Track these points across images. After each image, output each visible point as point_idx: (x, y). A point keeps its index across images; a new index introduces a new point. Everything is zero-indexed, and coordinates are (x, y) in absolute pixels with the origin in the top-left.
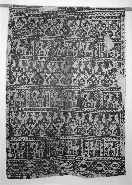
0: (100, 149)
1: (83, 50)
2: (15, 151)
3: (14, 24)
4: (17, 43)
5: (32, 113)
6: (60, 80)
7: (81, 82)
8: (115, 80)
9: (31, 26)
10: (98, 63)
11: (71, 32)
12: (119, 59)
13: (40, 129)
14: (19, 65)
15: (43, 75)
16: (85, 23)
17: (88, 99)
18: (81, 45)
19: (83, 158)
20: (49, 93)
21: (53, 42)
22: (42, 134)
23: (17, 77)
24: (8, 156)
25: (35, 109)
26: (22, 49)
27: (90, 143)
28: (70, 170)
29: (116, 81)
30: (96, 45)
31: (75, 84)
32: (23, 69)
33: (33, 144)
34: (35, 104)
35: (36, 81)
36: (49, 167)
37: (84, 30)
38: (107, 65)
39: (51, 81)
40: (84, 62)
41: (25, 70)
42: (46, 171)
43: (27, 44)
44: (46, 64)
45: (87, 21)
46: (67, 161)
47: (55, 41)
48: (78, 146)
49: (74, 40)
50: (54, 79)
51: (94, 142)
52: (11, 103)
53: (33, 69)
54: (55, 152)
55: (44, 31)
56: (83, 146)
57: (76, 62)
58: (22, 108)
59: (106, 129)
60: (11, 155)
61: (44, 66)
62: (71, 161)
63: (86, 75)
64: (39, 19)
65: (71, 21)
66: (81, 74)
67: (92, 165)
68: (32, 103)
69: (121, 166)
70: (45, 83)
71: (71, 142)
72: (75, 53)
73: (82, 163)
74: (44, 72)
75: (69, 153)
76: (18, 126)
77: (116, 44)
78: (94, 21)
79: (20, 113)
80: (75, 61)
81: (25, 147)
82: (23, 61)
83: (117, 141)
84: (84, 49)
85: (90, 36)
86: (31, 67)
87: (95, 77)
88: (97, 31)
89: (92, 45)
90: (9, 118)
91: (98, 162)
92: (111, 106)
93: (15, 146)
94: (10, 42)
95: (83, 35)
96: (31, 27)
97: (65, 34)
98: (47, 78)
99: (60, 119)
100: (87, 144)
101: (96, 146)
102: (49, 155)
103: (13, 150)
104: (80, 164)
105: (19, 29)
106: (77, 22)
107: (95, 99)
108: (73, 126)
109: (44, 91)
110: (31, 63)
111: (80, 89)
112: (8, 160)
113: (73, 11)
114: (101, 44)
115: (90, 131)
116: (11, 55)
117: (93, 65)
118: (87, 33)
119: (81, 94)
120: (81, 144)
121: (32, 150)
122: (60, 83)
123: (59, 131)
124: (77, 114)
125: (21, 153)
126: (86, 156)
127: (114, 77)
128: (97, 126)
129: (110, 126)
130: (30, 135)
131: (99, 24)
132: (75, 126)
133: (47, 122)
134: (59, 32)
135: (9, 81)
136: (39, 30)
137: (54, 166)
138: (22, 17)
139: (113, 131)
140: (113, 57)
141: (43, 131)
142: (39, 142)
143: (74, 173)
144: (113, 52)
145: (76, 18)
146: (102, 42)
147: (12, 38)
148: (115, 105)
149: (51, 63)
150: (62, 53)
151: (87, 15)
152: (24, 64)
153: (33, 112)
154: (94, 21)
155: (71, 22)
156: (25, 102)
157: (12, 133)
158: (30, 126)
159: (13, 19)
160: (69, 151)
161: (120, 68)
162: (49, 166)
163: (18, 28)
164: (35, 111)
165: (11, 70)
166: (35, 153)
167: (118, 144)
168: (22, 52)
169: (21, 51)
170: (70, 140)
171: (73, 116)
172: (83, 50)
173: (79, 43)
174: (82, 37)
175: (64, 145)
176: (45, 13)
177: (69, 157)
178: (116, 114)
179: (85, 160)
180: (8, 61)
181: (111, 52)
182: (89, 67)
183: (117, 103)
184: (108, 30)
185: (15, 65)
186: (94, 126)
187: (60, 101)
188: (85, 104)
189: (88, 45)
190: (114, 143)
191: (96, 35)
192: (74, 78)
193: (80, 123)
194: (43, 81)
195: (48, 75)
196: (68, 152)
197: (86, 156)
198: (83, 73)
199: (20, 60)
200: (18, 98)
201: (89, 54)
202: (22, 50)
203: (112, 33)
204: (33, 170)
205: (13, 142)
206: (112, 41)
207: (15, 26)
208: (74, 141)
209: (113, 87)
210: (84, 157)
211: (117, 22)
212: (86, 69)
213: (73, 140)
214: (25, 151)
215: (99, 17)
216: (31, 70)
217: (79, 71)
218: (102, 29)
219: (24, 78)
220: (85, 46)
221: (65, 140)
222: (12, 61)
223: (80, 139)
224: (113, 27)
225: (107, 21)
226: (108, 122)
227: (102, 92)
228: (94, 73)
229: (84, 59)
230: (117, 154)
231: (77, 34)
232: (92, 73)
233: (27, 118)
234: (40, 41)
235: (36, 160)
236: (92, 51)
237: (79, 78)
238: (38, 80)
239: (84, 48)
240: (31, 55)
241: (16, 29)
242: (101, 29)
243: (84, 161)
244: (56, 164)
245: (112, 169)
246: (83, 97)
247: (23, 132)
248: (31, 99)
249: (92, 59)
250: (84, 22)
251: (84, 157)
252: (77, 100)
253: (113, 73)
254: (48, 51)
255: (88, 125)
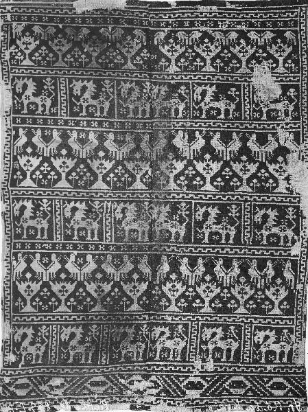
0: (240, 345)
1: (197, 103)
2: (24, 348)
3: (13, 42)
4: (25, 87)
5: (68, 255)
6: (138, 177)
7: (195, 182)
8: (286, 175)
9: (56, 45)
10: (238, 133)
11: (163, 60)
12: (295, 124)
13: (89, 294)
14: (35, 140)
15: (95, 164)
16: (202, 38)
17: (214, 223)
18: (194, 91)
19: (194, 368)
20: (111, 208)
21: (119, 84)
22: (93, 306)
23: (28, 170)
24: (4, 361)
25: (75, 247)
26: (38, 100)
27: (214, 330)
28: (157, 399)
29: (288, 179)
30: (292, 90)
31: (179, 185)
32: (45, 151)
33: (69, 330)
34: (76, 233)
35: (77, 178)
36: (103, 389)
37: (198, 55)
38: (262, 140)
39: (115, 179)
40: (201, 132)
41: (50, 152)
42: (96, 396)
43: (52, 90)
44: (101, 138)
45: (205, 34)
46: (150, 376)
47: (124, 81)
48: (183, 339)
49: (173, 79)
50: (51, 171)
51: (226, 329)
52: (15, 231)
53: (69, 149)
54: (124, 352)
55: (91, 56)
56: (197, 339)
57: (181, 134)
58: (42, 244)
59: (225, 294)
60: (12, 358)
61: (96, 142)
62: (161, 376)
63: (208, 165)
64: (78, 29)
65: (162, 33)
66: (195, 162)
67: (217, 381)
68: (69, 232)
69: (297, 387)
70: (100, 185)
71: (166, 330)
72: (177, 110)
73: (191, 379)
74: (97, 157)
75: (158, 358)
76: (67, 288)
77: (285, 89)
78: (225, 33)
79: (38, 256)
80: (177, 131)
81: (48, 337)
82: (43, 129)
83: (286, 328)
84: (201, 101)
85: (216, 67)
86: (64, 144)
87: (231, 167)
88: (234, 56)
89: (222, 90)
90: (10, 269)
91: (234, 375)
92: (274, 240)
93: (24, 336)
94: (7, 84)
95: (232, 68)
96: (58, 47)
97: (150, 66)
98: (104, 172)
99: (140, 273)
100: (208, 332)
101: (230, 338)
102: (106, 359)
103: (17, 345)
104: (186, 382)
105: (27, 52)
106: (180, 35)
107: (290, 225)
108: (173, 290)
109: (97, 203)
110: (65, 136)
111: (192, 198)
112: (4, 370)
113: (167, 10)
114: (244, 88)
115: (217, 301)
116: (12, 115)
117: (226, 138)
118: (208, 62)
119: (196, 211)
120: (191, 333)
121: (65, 344)
122: (138, 185)
123: (136, 301)
124: (186, 260)
125: (38, 352)
126: (204, 361)
127: (281, 168)
128: (234, 287)
129: (199, 286)
130: (62, 308)
131: (238, 39)
132: (177, 290)
133: (106, 279)
134: (133, 58)
135: (7, 180)
136: (78, 55)
137: (116, 385)
138: (34, 25)
139: (277, 303)
140: (280, 120)
141: (93, 299)
142: (85, 327)
143: (169, 404)
144: (279, 106)
145: (175, 27)
146: (249, 82)
147: (11, 74)
148: (286, 237)
149: (115, 134)
150: (144, 111)
151: (205, 19)
152: (47, 139)
153: (70, 254)
154: (225, 33)
155: (162, 35)
156: (50, 230)
157: (17, 304)
158: (63, 287)
159: (11, 28)
160: (158, 353)
161: (299, 144)
162: (103, 384)
163: (26, 51)
164: (75, 252)
165: (15, 154)
166: (72, 353)
167: (288, 335)
168: (40, 109)
169: (37, 106)
170: (165, 325)
171: (175, 266)
172: (197, 103)
173: (187, 85)
174: (193, 72)
175: (147, 336)
176: (93, 13)
177: (158, 366)
178: (286, 260)
179: (201, 372)
180: (7, 132)
181: (273, 106)
182: (215, 142)
183: (290, 233)
184: (265, 55)
185: (23, 140)
186: (229, 289)
187: (139, 229)
188: (206, 237)
189: (211, 90)
190: (279, 332)
191: (231, 65)
192: (175, 172)
193: (191, 282)
194: (96, 179)
195: (108, 165)
196: (155, 354)
197: (204, 361)
198: (200, 158)
199: (36, 129)
200: (31, 218)
201: (214, 112)
202: (40, 104)
203: (276, 61)
204: (65, 394)
205: (19, 327)
206: (275, 81)
207: (18, 47)
208: (172, 327)
209: (31, 187)
210: (198, 364)
211: (288, 34)
212: (208, 148)
213: (169, 324)
214: (47, 346)
215: (239, 23)
216: (64, 152)
217: (188, 154)
218: (176, 51)
219: (227, 177)
220: (204, 94)
221: (151, 326)
222: (16, 129)
223: (190, 322)
224: (205, 45)
225: (259, 32)
226: (265, 280)
227: (250, 205)
228: (228, 158)
229: (200, 126)
230: (285, 360)
231: (66, 59)
232: (45, 155)
233: (56, 267)
234: (82, 82)
235: (72, 369)
236: (221, 105)
237: (190, 171)
238: (82, 176)
239: (200, 98)
240: (63, 115)
241: (19, 54)
242: (172, 50)
243: (197, 373)
244: (123, 381)
245: (272, 395)
246: (201, 218)
247: (45, 302)
248: (67, 220)
249: (224, 124)
250: (197, 35)
251: (198, 364)
252: (184, 225)
253: (280, 159)
254: (107, 105)
255: (179, 286)
